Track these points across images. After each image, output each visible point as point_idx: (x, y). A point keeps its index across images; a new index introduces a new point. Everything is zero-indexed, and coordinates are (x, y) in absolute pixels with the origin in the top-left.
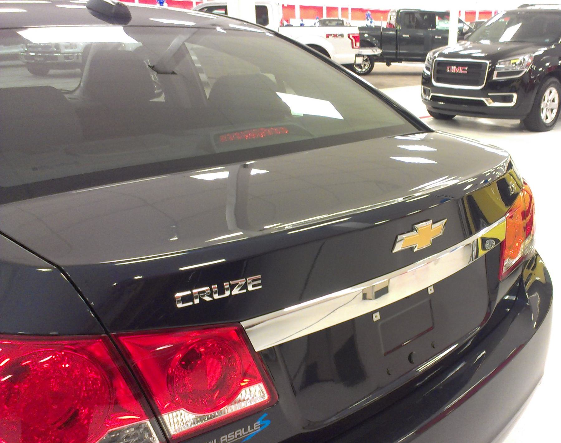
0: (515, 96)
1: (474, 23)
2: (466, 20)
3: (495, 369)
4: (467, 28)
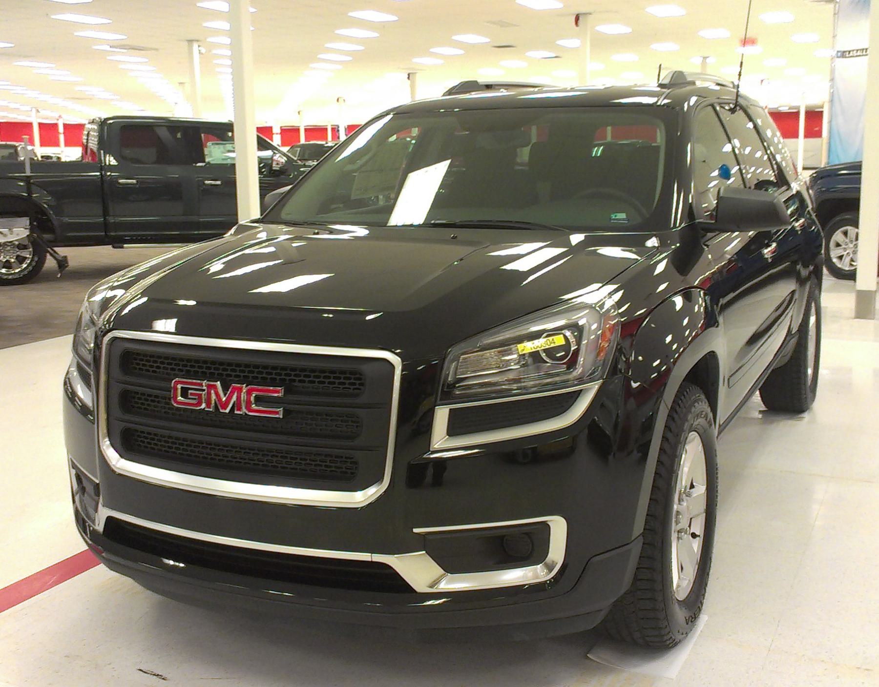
0: (558, 527)
1: (298, 147)
2: (284, 144)
3: (723, 263)
4: (283, 160)
